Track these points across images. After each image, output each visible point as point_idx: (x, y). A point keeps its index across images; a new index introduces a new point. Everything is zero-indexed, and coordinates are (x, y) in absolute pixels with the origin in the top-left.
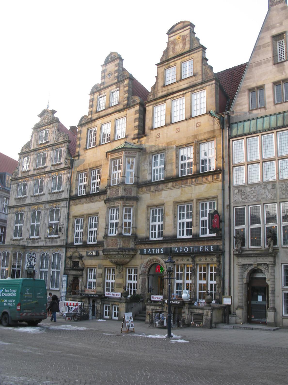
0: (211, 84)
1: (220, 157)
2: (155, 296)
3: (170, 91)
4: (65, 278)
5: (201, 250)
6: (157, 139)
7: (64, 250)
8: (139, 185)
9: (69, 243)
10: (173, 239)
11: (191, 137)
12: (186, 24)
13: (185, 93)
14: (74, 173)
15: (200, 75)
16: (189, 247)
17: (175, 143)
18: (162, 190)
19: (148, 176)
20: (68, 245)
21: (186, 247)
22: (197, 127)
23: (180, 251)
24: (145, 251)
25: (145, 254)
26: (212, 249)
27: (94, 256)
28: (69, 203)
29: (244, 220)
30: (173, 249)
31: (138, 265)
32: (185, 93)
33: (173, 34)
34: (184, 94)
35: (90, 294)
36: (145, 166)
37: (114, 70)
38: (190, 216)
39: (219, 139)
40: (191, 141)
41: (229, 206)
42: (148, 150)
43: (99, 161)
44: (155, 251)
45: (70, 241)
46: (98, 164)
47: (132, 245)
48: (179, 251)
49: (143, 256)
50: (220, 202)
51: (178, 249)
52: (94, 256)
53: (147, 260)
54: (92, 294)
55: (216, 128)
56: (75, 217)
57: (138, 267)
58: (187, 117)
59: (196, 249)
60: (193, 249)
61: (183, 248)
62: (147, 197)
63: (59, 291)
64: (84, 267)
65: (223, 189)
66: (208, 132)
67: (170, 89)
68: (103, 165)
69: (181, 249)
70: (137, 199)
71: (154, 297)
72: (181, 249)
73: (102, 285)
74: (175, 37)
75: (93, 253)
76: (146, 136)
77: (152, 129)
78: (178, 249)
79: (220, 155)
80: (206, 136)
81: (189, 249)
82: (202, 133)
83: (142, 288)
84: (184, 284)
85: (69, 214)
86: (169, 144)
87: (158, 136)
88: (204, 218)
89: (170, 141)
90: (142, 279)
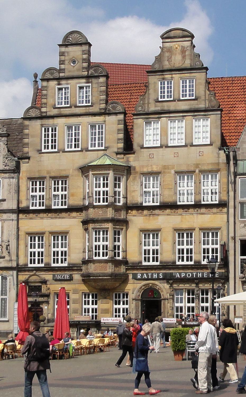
0: (216, 114)
1: (225, 191)
2: (167, 319)
3: (166, 108)
5: (206, 276)
6: (150, 160)
7: (15, 272)
8: (128, 208)
9: (21, 264)
10: (173, 266)
12: (186, 33)
13: (186, 116)
14: (22, 179)
16: (192, 273)
18: (158, 215)
19: (139, 197)
20: (19, 266)
21: (189, 274)
22: (199, 155)
23: (182, 276)
24: (139, 275)
25: (139, 279)
27: (229, 165)
28: (18, 216)
30: (174, 275)
31: (130, 290)
32: (186, 116)
33: (169, 40)
34: (183, 116)
35: (82, 322)
36: (135, 187)
37: (80, 57)
39: (224, 172)
40: (192, 169)
41: (234, 238)
42: (138, 169)
43: (65, 170)
44: (152, 275)
45: (21, 262)
46: (63, 174)
47: (122, 269)
48: (180, 276)
49: (136, 281)
50: (225, 233)
51: (180, 274)
52: (229, 165)
54: (86, 321)
55: (221, 161)
58: (187, 143)
59: (200, 275)
60: (197, 275)
61: (186, 273)
62: (138, 221)
63: (8, 321)
64: (50, 293)
65: (228, 221)
66: (212, 164)
67: (166, 106)
68: (72, 176)
69: (183, 275)
70: (125, 222)
71: (165, 320)
72: (183, 275)
73: (79, 311)
76: (134, 153)
77: (142, 147)
78: (180, 274)
79: (225, 189)
80: (210, 167)
81: (193, 275)
82: (205, 164)
83: (136, 312)
84: (185, 307)
85: (18, 228)
86: (165, 167)
87: (151, 156)
88: (215, 245)
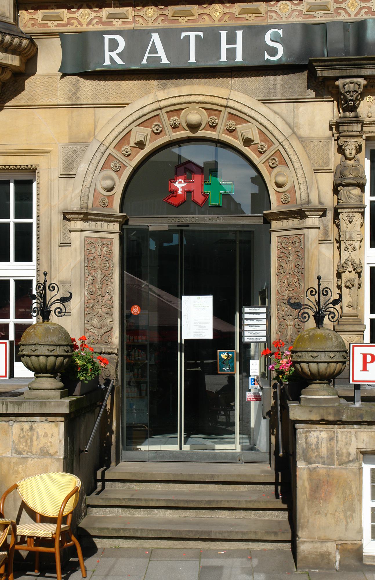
24: (114, 45)
44: (209, 40)
53: (128, 110)
57: (41, 163)
90: (90, 243)
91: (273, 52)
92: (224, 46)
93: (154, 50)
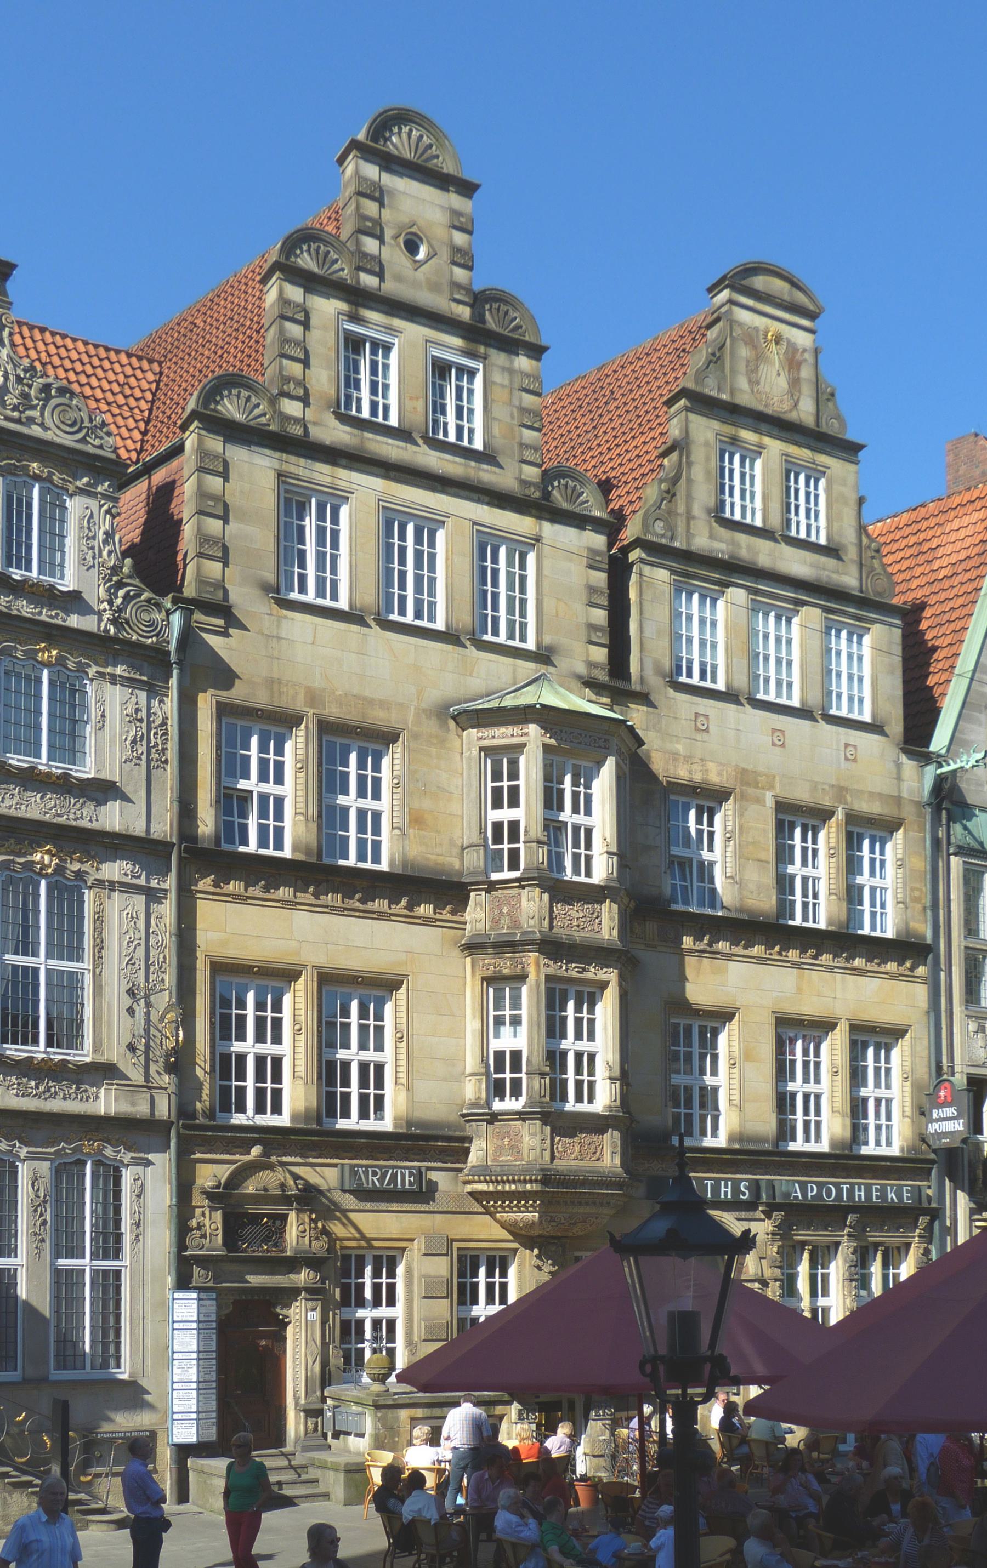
4: (187, 1307)
5: (877, 1197)
6: (699, 737)
11: (826, 787)
15: (852, 561)
16: (837, 1185)
17: (772, 787)
23: (810, 1194)
26: (908, 1198)
29: (72, 1258)
38: (375, 1113)
43: (384, 705)
46: (379, 718)
48: (804, 1194)
56: (219, 968)
69: (812, 1190)
74: (760, 321)
75: (394, 1176)
89: (750, 767)
91: (744, 1194)
92: (723, 1189)
93: (796, 1192)
